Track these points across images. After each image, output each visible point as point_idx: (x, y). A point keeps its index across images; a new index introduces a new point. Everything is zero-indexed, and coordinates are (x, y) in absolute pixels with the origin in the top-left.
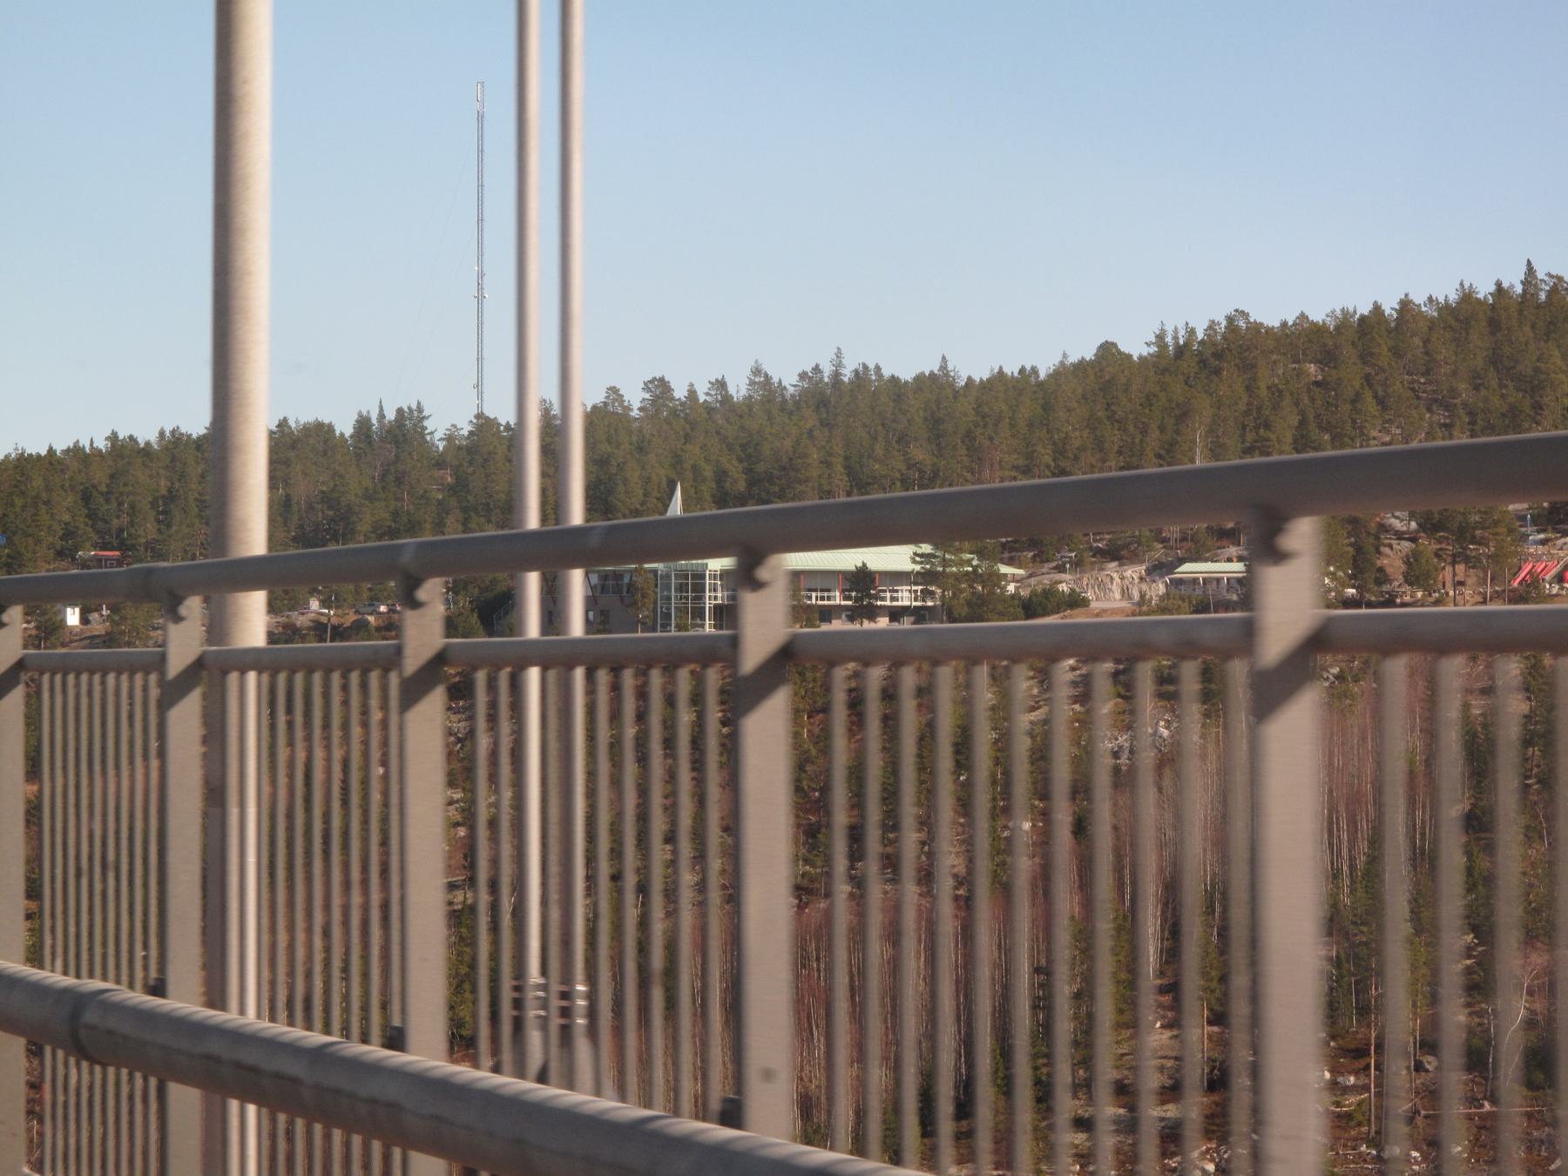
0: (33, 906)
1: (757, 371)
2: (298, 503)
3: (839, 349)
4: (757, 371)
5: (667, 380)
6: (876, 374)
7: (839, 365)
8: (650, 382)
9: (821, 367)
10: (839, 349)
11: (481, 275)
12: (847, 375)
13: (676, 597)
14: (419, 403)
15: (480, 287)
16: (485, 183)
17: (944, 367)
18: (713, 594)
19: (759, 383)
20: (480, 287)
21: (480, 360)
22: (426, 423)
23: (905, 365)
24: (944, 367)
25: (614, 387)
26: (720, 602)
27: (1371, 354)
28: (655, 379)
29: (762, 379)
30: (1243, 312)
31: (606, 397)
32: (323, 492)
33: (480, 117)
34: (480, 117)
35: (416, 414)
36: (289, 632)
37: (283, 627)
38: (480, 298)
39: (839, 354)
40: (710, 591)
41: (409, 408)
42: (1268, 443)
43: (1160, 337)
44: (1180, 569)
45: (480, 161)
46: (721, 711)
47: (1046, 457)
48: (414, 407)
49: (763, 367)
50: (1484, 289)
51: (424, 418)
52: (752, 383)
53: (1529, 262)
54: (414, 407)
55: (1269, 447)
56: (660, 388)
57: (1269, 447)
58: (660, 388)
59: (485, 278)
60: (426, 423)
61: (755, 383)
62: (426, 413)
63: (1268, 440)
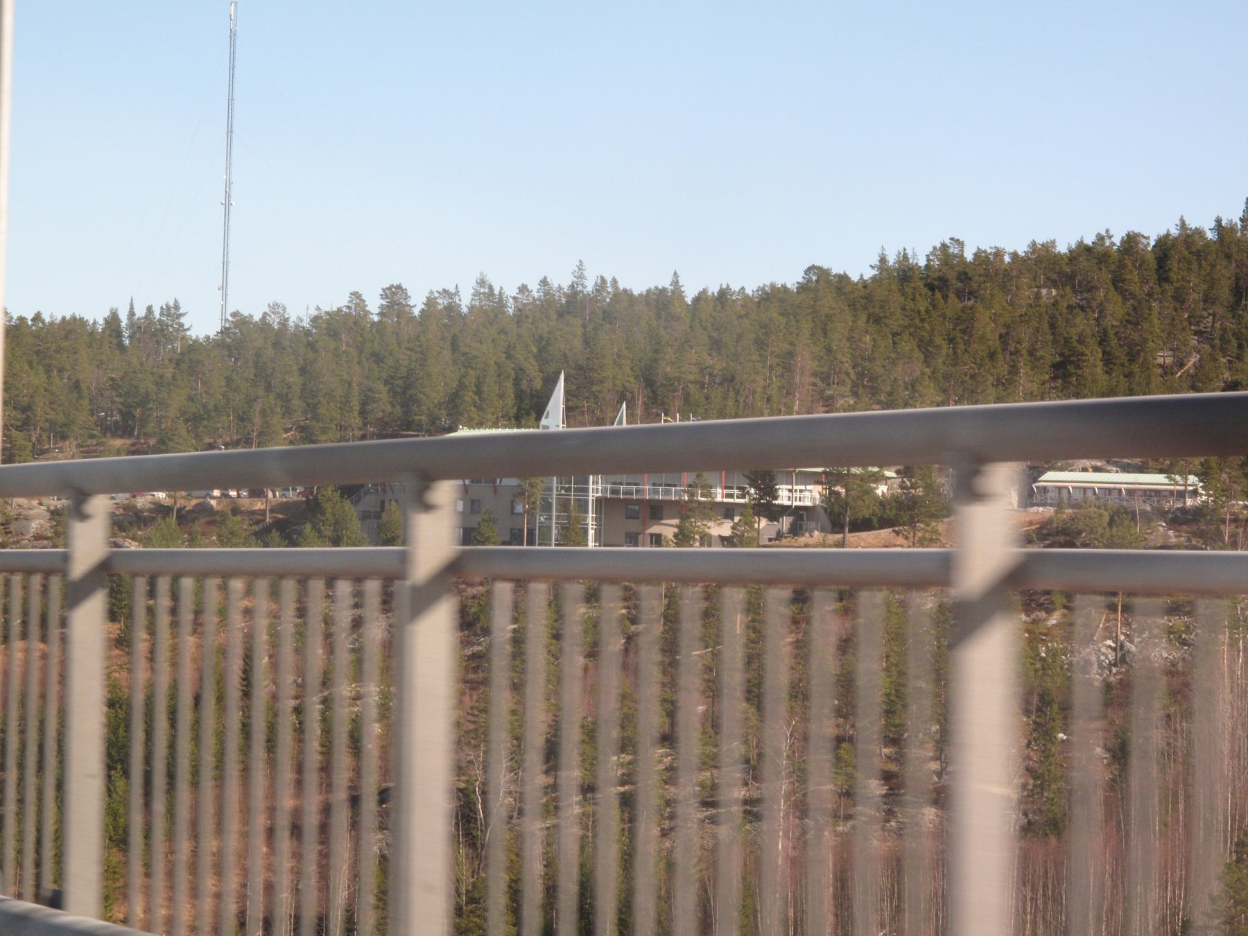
0: (116, 856)
1: (482, 283)
2: (89, 388)
3: (581, 261)
4: (482, 283)
5: (404, 287)
6: (613, 287)
7: (580, 276)
8: (389, 289)
9: (548, 280)
10: (581, 261)
11: (229, 183)
12: (589, 286)
13: (557, 488)
14: (176, 301)
15: (228, 195)
16: (235, 97)
17: (675, 283)
18: (595, 487)
19: (484, 293)
20: (228, 195)
21: (225, 264)
22: (182, 320)
23: (638, 282)
24: (675, 283)
25: (357, 293)
26: (600, 495)
27: (1124, 281)
28: (392, 286)
29: (487, 290)
30: (958, 240)
31: (350, 302)
32: (113, 379)
33: (233, 35)
34: (233, 35)
35: (173, 311)
36: (130, 513)
37: (124, 509)
38: (227, 206)
39: (581, 266)
40: (593, 484)
41: (167, 305)
42: (1084, 358)
43: (883, 260)
44: (1044, 477)
45: (232, 77)
46: (624, 608)
47: (846, 365)
48: (171, 304)
49: (487, 278)
50: (683, 289)
51: (181, 315)
52: (476, 294)
53: (675, 274)
54: (171, 304)
55: (1084, 361)
56: (395, 295)
57: (1084, 361)
58: (395, 295)
59: (232, 186)
60: (182, 320)
61: (480, 293)
62: (181, 311)
63: (1082, 354)
